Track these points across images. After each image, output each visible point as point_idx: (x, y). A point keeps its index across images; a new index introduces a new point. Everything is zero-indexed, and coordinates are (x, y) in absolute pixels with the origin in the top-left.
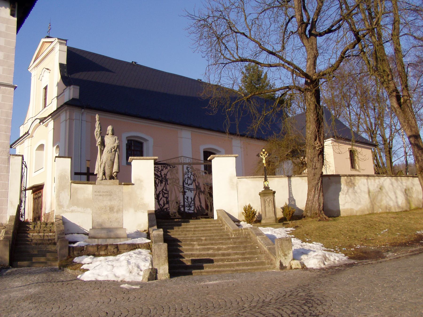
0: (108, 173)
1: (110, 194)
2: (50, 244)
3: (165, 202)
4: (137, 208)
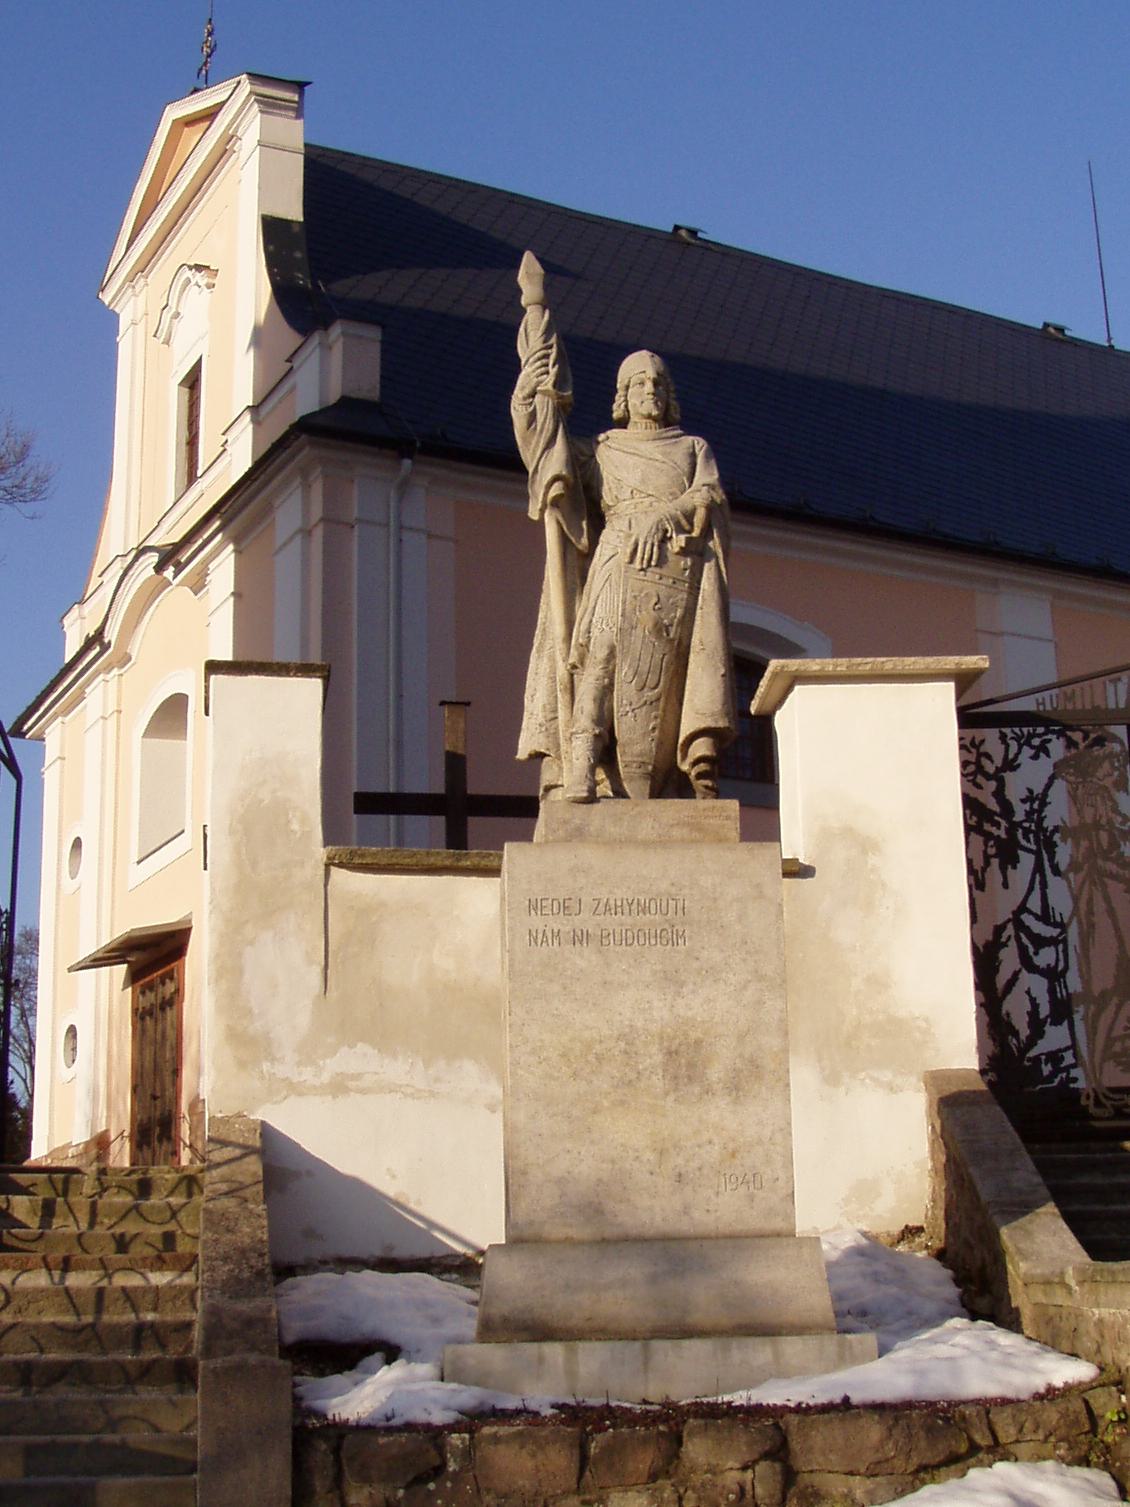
0: (635, 741)
1: (663, 926)
2: (147, 1373)
3: (1044, 1010)
4: (851, 1053)
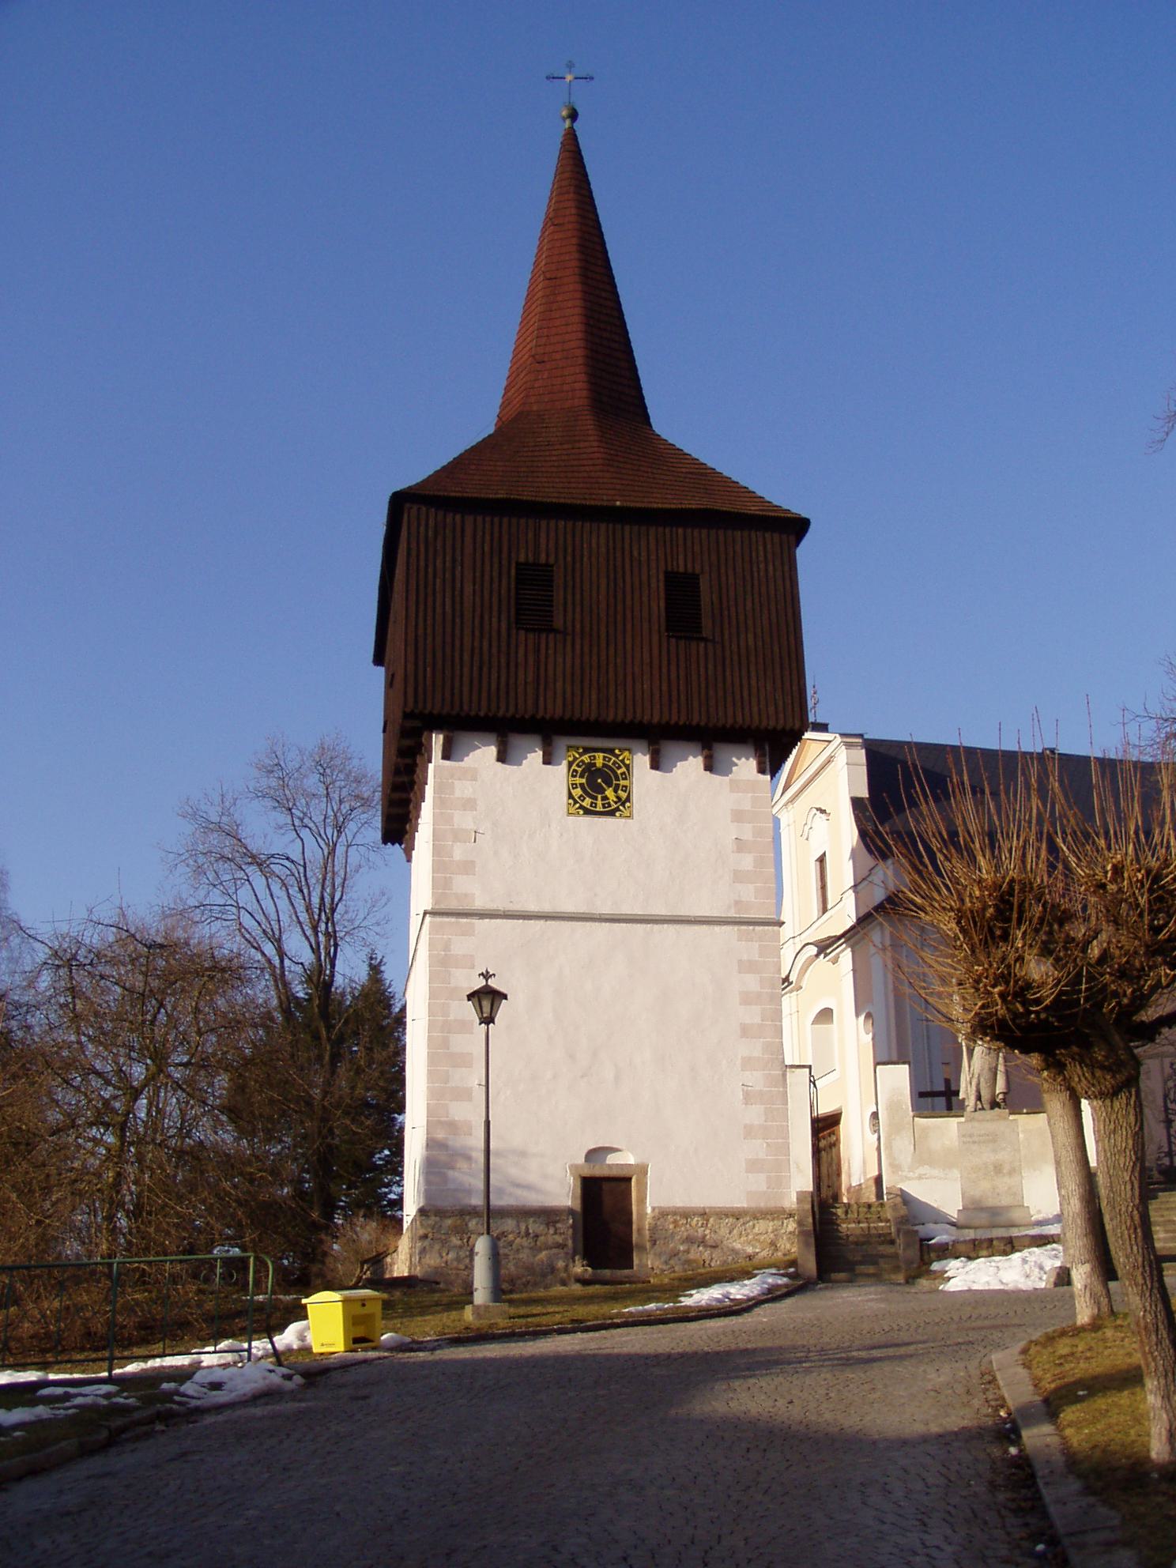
1: (992, 1139)
